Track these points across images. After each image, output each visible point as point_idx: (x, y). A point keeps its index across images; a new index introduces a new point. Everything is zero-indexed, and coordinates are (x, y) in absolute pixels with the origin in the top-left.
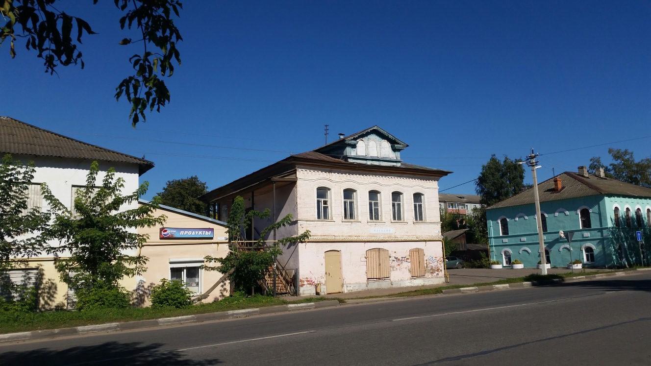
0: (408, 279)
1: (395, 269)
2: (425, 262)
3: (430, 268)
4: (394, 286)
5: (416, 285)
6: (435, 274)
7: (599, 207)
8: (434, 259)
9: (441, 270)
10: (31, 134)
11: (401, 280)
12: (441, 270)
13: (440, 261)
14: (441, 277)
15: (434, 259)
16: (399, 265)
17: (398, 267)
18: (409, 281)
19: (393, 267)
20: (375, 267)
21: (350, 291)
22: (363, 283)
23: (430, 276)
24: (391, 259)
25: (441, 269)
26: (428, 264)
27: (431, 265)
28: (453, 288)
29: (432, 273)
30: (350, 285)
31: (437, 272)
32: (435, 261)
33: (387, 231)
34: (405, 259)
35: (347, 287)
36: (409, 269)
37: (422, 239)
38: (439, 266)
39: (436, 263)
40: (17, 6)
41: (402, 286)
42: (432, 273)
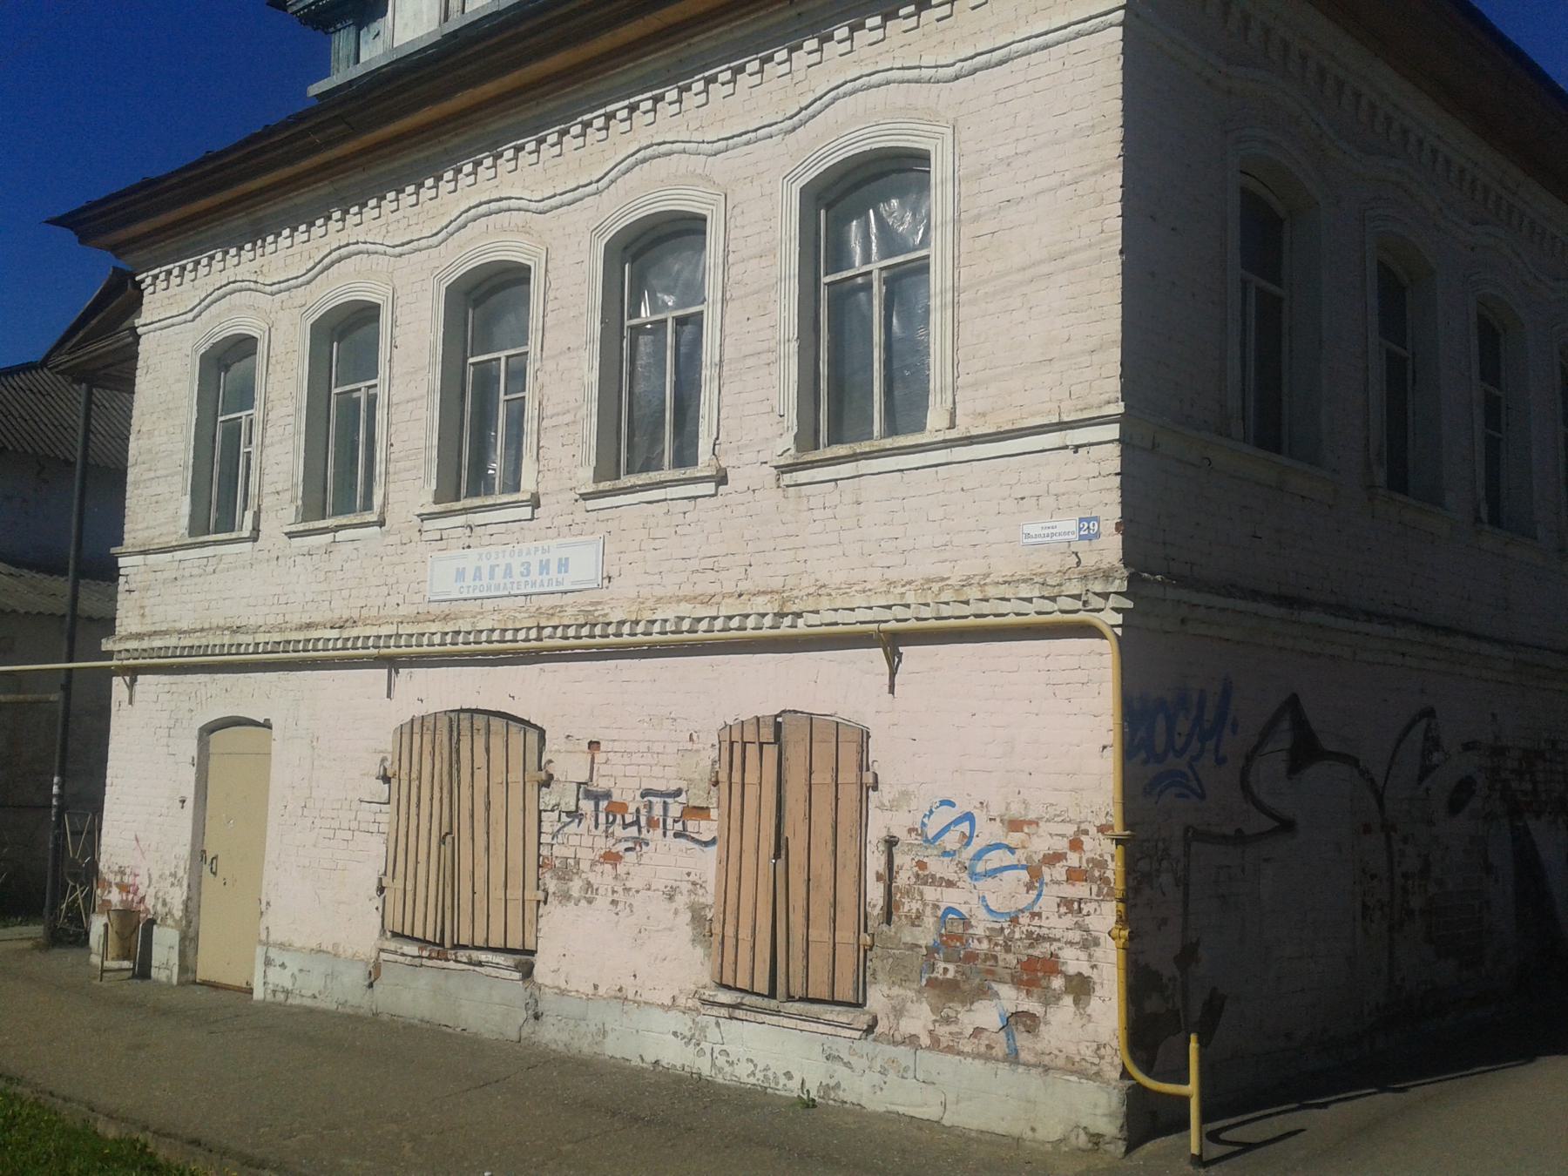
0: (674, 1004)
1: (576, 886)
2: (875, 862)
3: (926, 935)
4: (551, 1034)
5: (743, 1073)
6: (987, 1015)
7: (172, 927)
8: (988, 832)
9: (1081, 987)
10: (597, 610)
11: (620, 997)
12: (1081, 987)
13: (1074, 875)
14: (1075, 1068)
15: (988, 832)
16: (612, 858)
17: (603, 877)
18: (682, 1023)
19: (565, 872)
20: (422, 857)
21: (281, 997)
22: (353, 959)
23: (919, 1018)
24: (549, 798)
25: (1074, 961)
26: (903, 879)
27: (950, 898)
28: (1230, 595)
29: (947, 991)
30: (286, 958)
31: (1010, 998)
32: (996, 859)
33: (544, 567)
34: (675, 810)
35: (268, 962)
36: (698, 917)
37: (848, 621)
38: (1056, 923)
39: (1008, 891)
40: (589, 472)
41: (614, 1048)
42: (947, 991)
